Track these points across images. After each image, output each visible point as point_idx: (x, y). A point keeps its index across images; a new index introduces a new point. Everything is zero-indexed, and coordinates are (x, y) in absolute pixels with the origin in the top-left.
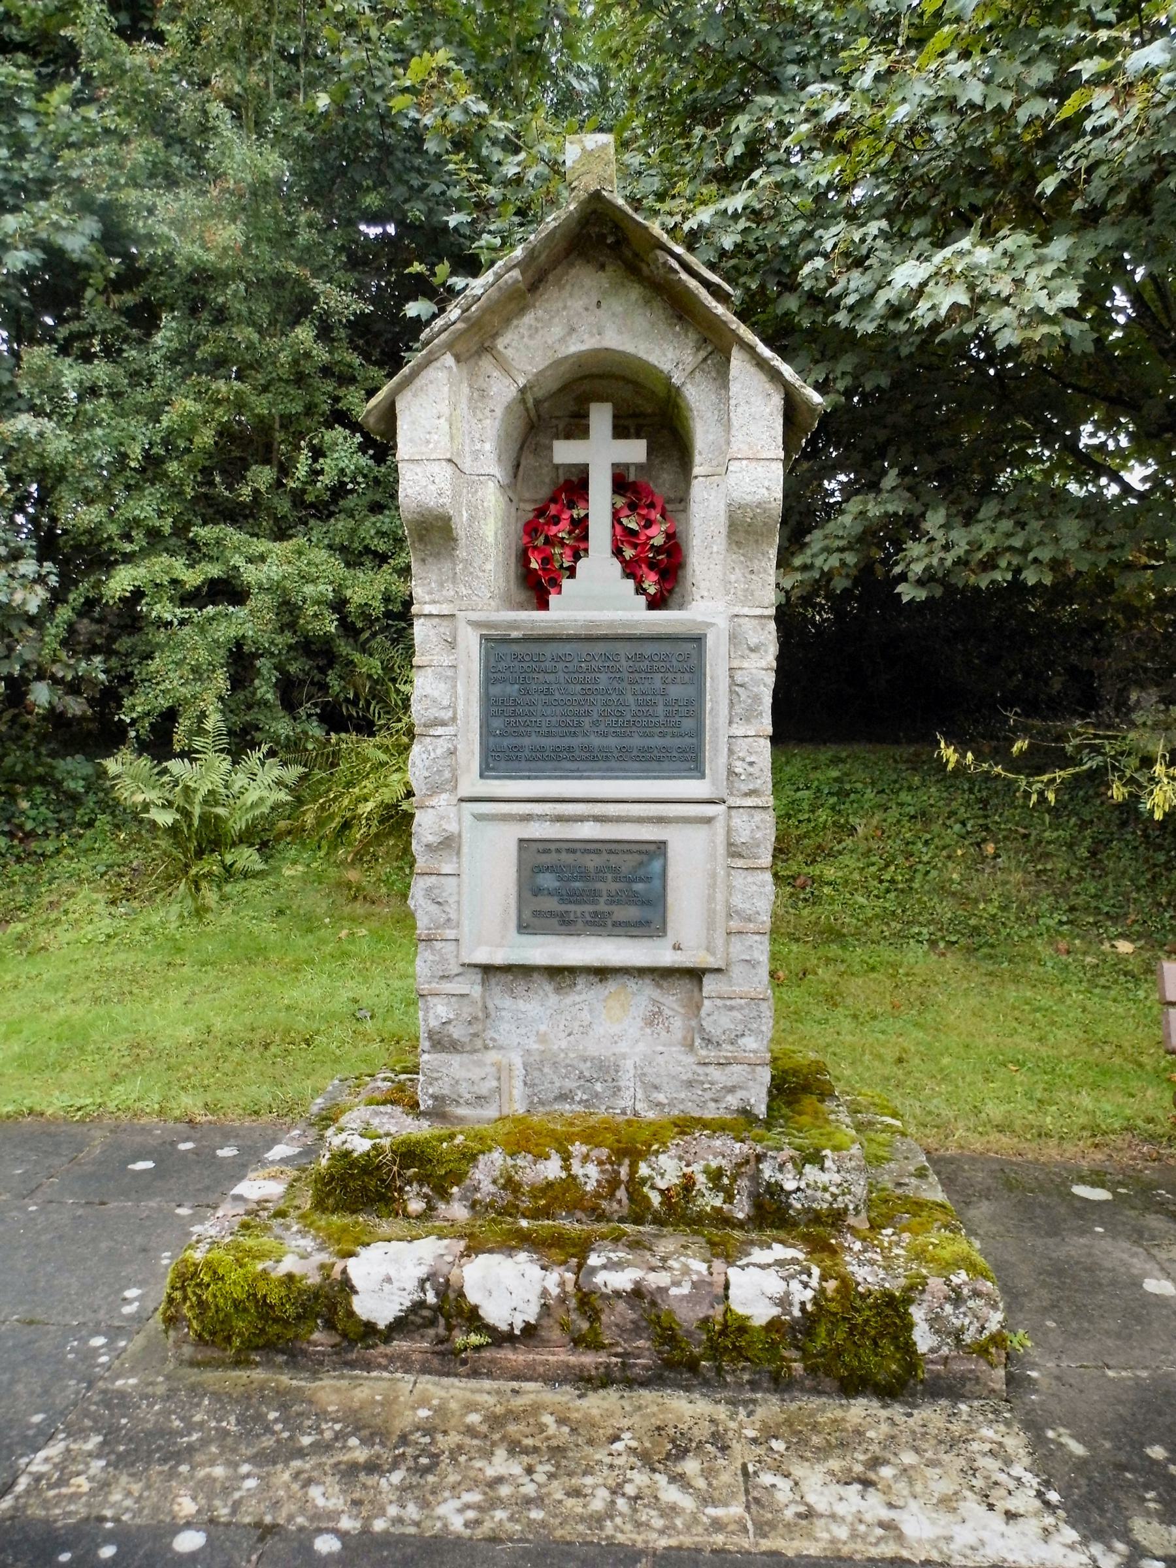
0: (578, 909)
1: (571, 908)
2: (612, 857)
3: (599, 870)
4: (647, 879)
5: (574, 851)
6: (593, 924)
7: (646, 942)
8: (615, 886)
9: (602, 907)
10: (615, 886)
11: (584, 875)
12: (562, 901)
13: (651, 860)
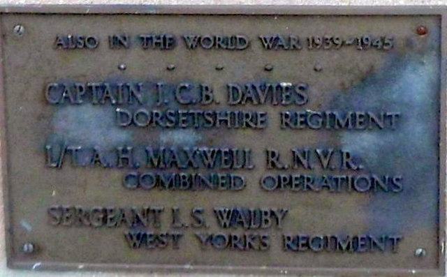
0: (182, 201)
1: (162, 200)
2: (278, 60)
6: (231, 243)
8: (286, 142)
9: (252, 198)
11: (193, 108)
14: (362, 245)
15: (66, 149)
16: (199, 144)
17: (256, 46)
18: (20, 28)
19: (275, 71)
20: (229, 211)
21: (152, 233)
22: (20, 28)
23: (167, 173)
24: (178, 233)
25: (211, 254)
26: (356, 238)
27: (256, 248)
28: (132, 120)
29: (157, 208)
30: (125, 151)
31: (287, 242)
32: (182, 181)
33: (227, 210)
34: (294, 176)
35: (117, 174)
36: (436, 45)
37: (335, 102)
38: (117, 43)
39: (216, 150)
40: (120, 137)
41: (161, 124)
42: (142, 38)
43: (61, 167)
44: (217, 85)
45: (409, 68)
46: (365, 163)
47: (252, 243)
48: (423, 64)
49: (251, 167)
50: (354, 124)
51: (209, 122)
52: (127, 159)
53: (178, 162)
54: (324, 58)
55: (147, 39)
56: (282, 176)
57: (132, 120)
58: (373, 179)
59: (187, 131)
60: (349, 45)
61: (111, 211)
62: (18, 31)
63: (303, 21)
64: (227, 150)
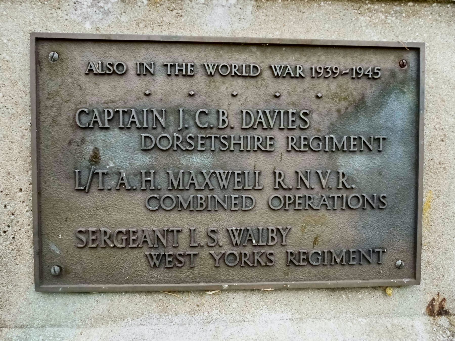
0: (202, 223)
1: (182, 221)
2: (285, 87)
3: (256, 121)
4: (372, 144)
5: (185, 72)
6: (241, 262)
7: (371, 301)
8: (292, 164)
9: (260, 218)
10: (292, 164)
11: (210, 133)
12: (157, 203)
13: (385, 93)
14: (353, 258)
15: (93, 173)
16: (214, 166)
17: (267, 74)
18: (53, 54)
19: (283, 97)
20: (241, 230)
21: (171, 253)
22: (53, 54)
23: (185, 194)
24: (195, 252)
25: (224, 272)
26: (348, 252)
27: (263, 264)
28: (156, 144)
29: (175, 229)
30: (148, 174)
31: (290, 257)
32: (199, 202)
33: (239, 229)
34: (297, 196)
35: (140, 198)
36: (414, 76)
37: (332, 128)
38: (145, 71)
39: (230, 172)
40: (143, 160)
41: (182, 147)
42: (166, 65)
43: (89, 190)
44: (232, 109)
45: (393, 96)
46: (356, 183)
47: (260, 260)
48: (404, 93)
49: (260, 188)
50: (349, 146)
51: (225, 145)
52: (149, 181)
53: (196, 183)
54: (324, 87)
55: (171, 65)
56: (287, 196)
57: (156, 144)
58: (363, 197)
59: (204, 154)
60: (345, 73)
61: (134, 232)
62: (52, 57)
63: (308, 51)
64: (240, 172)
